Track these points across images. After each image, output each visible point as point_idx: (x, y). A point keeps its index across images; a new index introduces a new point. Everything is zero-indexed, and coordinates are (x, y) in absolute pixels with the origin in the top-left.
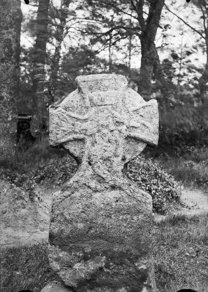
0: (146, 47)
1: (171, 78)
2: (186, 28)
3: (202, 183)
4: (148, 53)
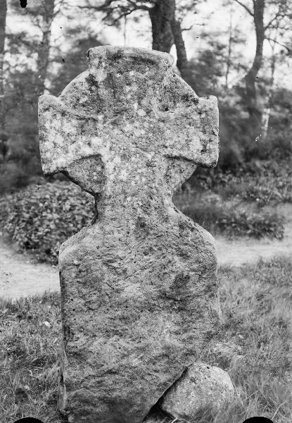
0: (158, 28)
1: (43, 77)
2: (92, 11)
3: (225, 226)
4: (162, 36)
